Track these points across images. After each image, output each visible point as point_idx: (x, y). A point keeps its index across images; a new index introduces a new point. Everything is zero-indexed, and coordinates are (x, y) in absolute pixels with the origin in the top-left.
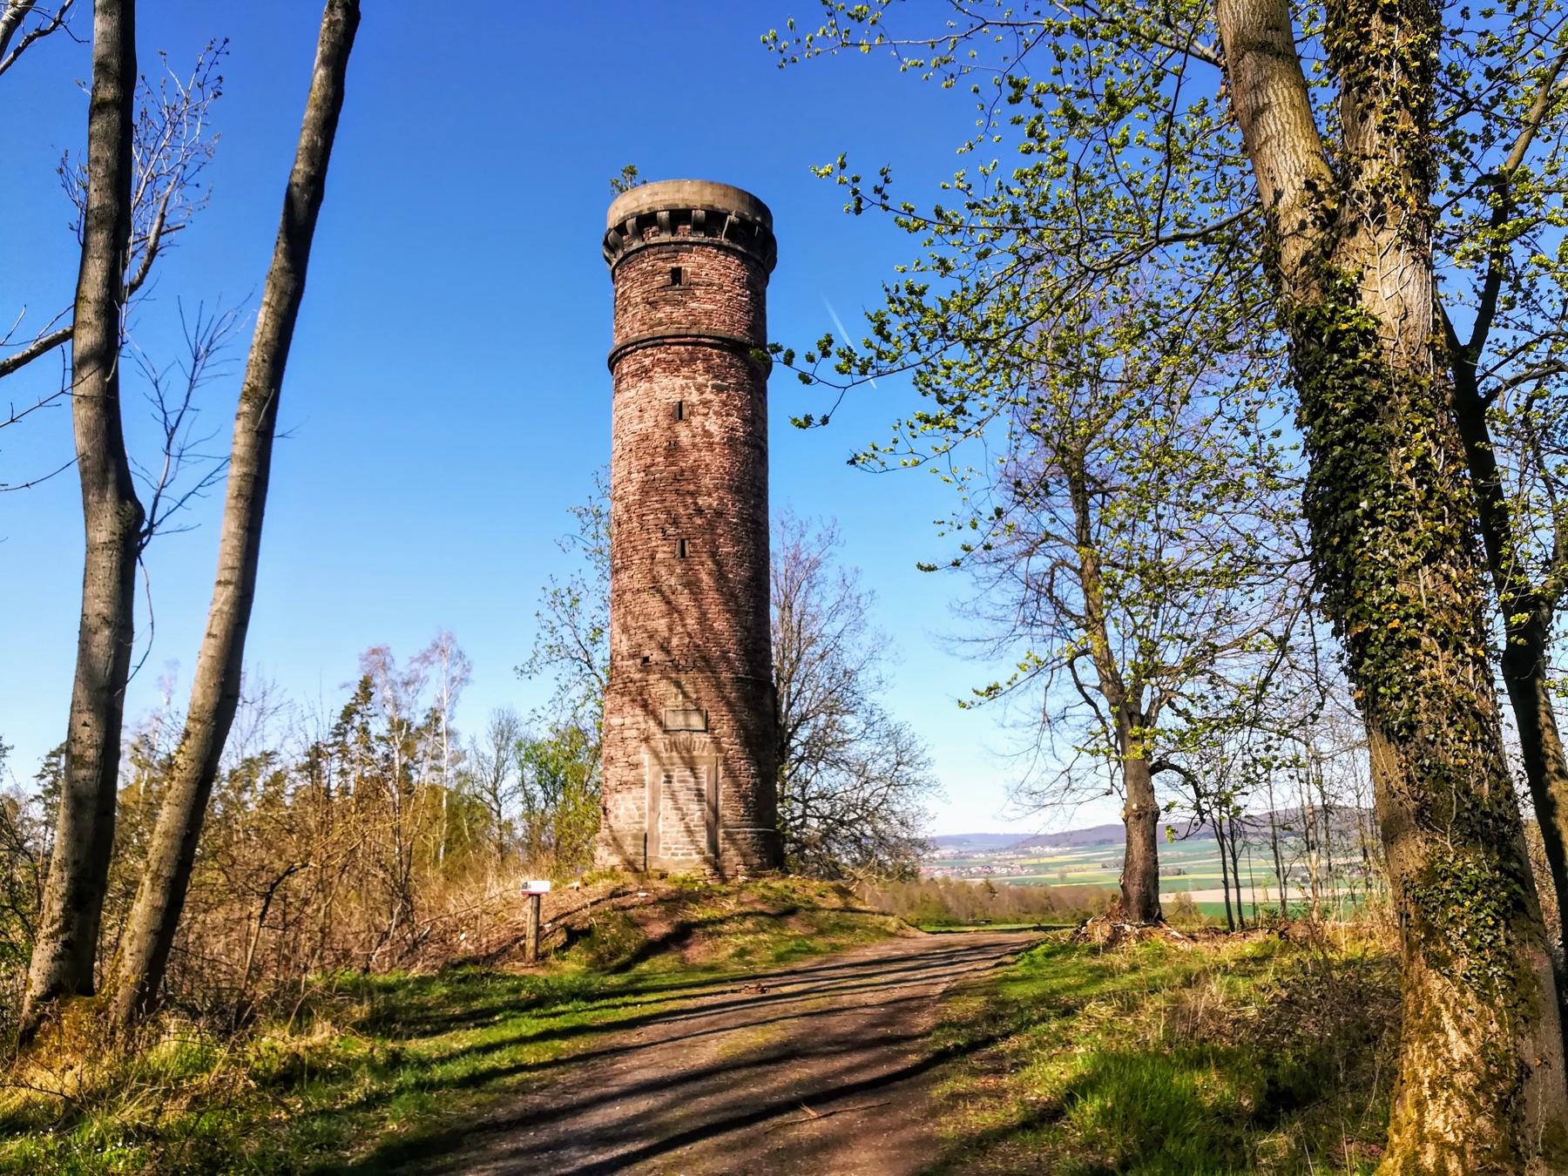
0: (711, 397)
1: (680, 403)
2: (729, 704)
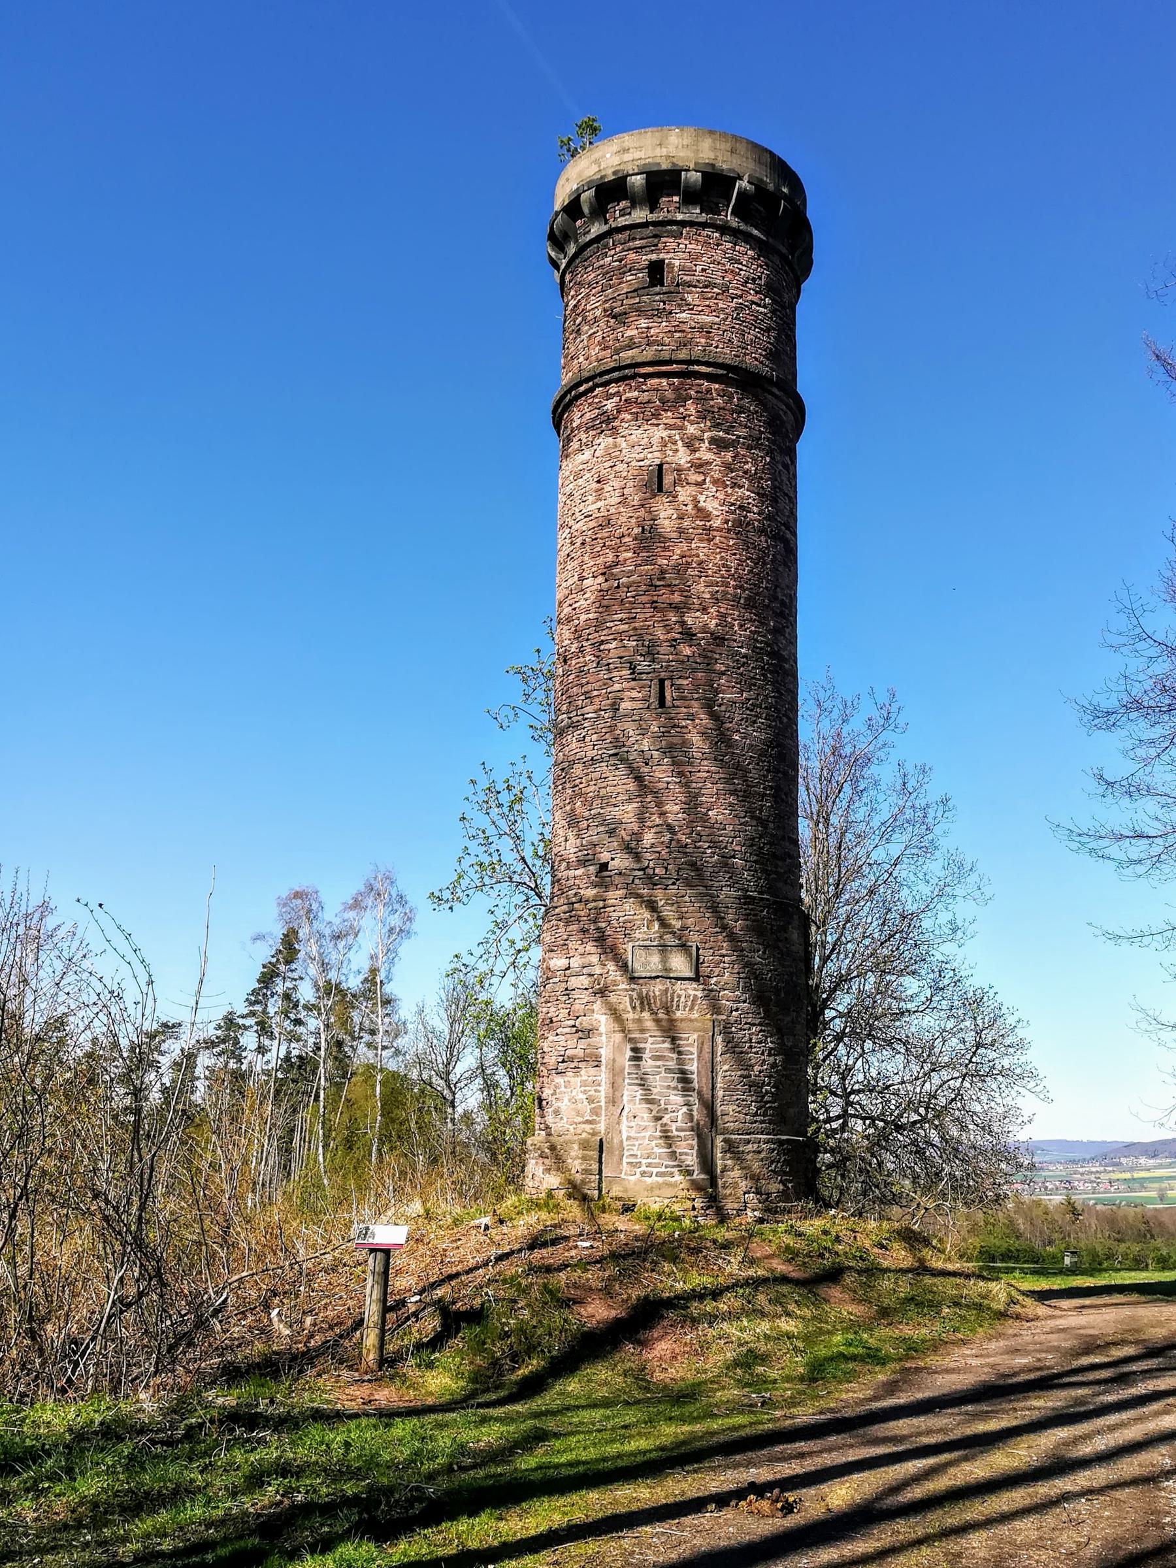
0: (708, 456)
1: (660, 466)
2: (732, 937)
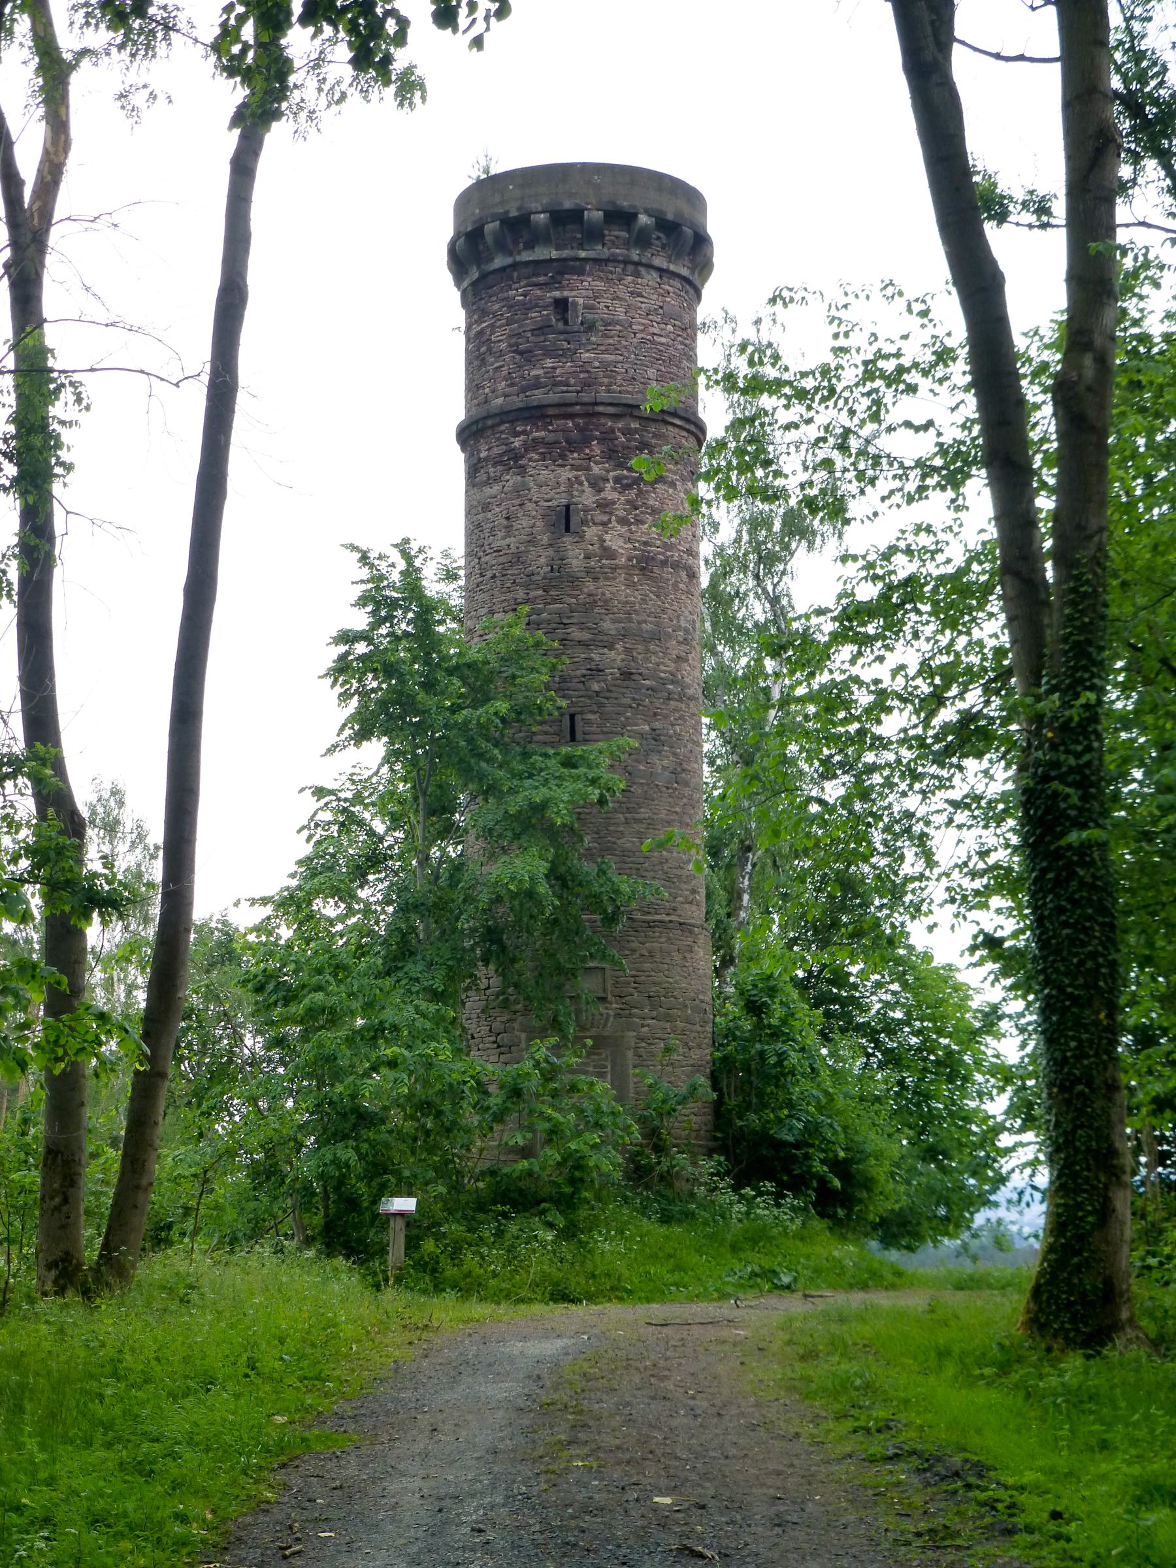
0: (614, 496)
1: (568, 507)
